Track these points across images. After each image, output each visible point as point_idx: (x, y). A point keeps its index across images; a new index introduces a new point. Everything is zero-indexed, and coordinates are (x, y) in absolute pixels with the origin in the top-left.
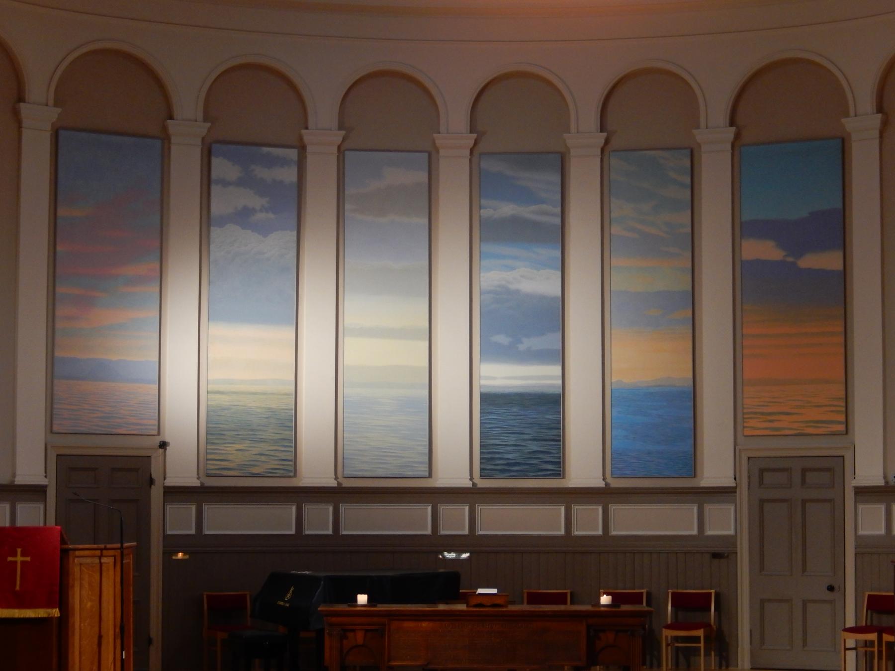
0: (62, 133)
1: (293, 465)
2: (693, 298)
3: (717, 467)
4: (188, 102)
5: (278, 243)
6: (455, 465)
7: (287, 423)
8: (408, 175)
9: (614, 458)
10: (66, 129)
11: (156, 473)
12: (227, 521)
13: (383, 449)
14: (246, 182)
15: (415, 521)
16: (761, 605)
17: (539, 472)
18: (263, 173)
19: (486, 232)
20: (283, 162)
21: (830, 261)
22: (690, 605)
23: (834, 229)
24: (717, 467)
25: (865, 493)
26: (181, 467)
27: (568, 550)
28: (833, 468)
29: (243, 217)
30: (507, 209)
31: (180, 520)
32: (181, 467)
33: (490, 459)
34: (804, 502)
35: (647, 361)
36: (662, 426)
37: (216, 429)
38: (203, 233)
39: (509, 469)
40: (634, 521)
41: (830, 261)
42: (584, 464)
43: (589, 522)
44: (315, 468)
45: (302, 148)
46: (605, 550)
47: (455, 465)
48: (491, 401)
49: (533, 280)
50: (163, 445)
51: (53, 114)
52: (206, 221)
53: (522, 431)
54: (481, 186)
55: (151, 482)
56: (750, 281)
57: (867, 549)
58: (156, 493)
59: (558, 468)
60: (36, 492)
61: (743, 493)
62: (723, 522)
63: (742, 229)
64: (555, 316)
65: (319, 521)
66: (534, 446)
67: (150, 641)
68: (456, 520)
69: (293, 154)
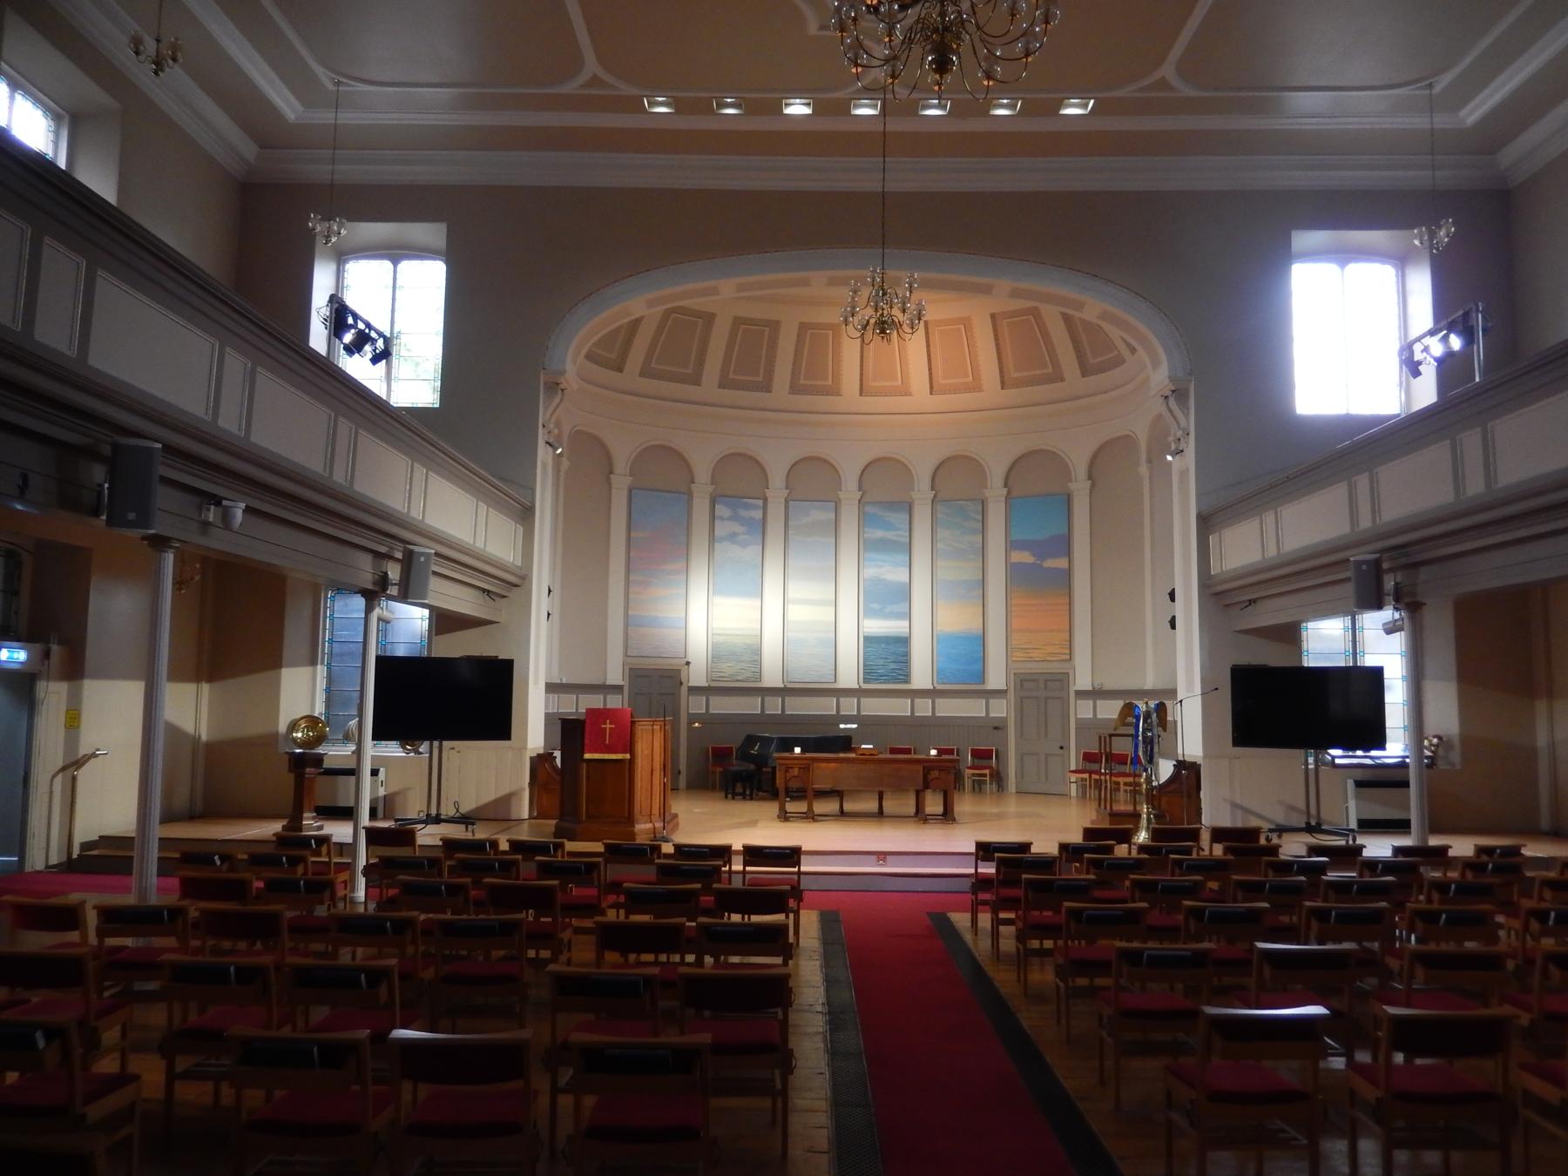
3: (996, 679)
4: (703, 473)
5: (751, 552)
6: (849, 676)
7: (756, 652)
8: (823, 514)
9: (938, 673)
13: (809, 669)
14: (734, 518)
17: (896, 680)
18: (743, 513)
19: (867, 547)
20: (755, 507)
21: (1061, 563)
22: (981, 755)
23: (1064, 545)
24: (996, 679)
25: (1081, 694)
26: (697, 676)
28: (1063, 680)
29: (732, 537)
30: (879, 534)
31: (697, 705)
33: (869, 673)
35: (957, 619)
37: (717, 655)
40: (949, 708)
41: (1061, 563)
42: (921, 676)
43: (924, 708)
44: (771, 679)
45: (765, 500)
47: (849, 676)
48: (870, 640)
49: (890, 571)
50: (688, 663)
51: (629, 480)
52: (712, 539)
53: (887, 658)
54: (864, 520)
57: (1082, 726)
58: (684, 690)
59: (907, 678)
60: (617, 689)
61: (1011, 694)
62: (1000, 709)
63: (1011, 545)
64: (905, 593)
65: (774, 706)
66: (893, 666)
69: (760, 502)
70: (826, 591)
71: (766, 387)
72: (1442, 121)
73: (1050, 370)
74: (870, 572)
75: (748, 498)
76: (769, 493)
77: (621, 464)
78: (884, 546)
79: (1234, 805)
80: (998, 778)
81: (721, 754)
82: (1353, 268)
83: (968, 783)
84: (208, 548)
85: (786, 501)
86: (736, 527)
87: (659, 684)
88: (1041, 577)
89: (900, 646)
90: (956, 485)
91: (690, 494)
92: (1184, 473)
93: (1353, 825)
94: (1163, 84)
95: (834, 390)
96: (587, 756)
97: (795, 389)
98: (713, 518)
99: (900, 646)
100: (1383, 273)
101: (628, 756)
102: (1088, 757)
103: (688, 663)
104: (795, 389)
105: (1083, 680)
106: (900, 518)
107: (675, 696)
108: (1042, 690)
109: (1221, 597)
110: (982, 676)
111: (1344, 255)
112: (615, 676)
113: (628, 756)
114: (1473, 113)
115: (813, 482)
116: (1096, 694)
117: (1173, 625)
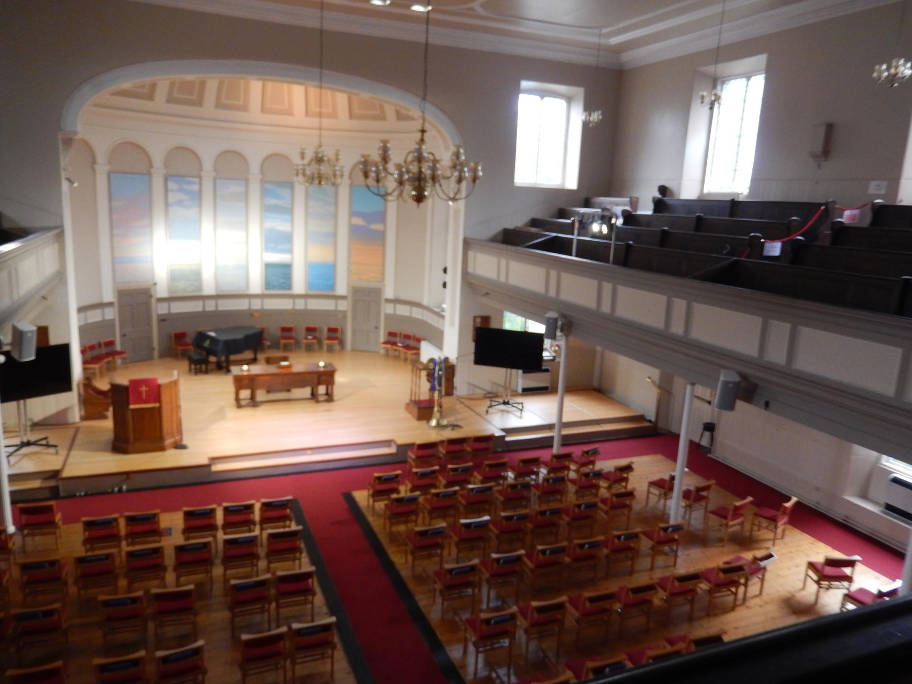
0: (112, 175)
1: (200, 288)
2: (335, 235)
3: (342, 289)
4: (158, 160)
5: (192, 212)
6: (256, 285)
7: (198, 274)
8: (236, 188)
9: (309, 285)
10: (113, 172)
11: (153, 292)
12: (179, 308)
13: (231, 284)
14: (181, 190)
15: (241, 305)
16: (354, 332)
17: (284, 288)
18: (186, 187)
19: (267, 209)
20: (194, 183)
21: (379, 227)
22: (332, 330)
23: (381, 217)
24: (342, 289)
25: (388, 301)
26: (162, 291)
27: (294, 313)
28: (377, 293)
29: (180, 203)
30: (273, 201)
31: (162, 309)
32: (162, 291)
33: (268, 285)
34: (263, 110)
35: (320, 254)
36: (323, 277)
37: (173, 277)
38: (348, 471)
39: (274, 288)
40: (315, 305)
41: (379, 227)
42: (299, 285)
43: (300, 305)
44: (209, 289)
45: (200, 177)
46: (305, 313)
47: (256, 285)
48: (268, 266)
49: (280, 225)
50: (155, 284)
51: (107, 168)
52: (167, 204)
53: (278, 276)
54: (264, 193)
55: (151, 296)
56: (356, 232)
57: (388, 317)
58: (153, 301)
59: (289, 286)
60: (110, 304)
61: (350, 298)
62: (343, 306)
63: (353, 214)
64: (288, 238)
65: (210, 306)
66: (282, 281)
67: (153, 349)
68: (256, 305)
69: (197, 180)
70: (241, 235)
71: (199, 102)
72: (603, 41)
73: (379, 112)
74: (269, 224)
75: (187, 177)
76: (203, 174)
77: (101, 158)
78: (276, 209)
79: (470, 384)
80: (342, 343)
81: (180, 337)
82: (546, 99)
83: (325, 347)
84: (43, 534)
85: (215, 180)
86: (181, 196)
87: (136, 300)
88: (367, 235)
89: (285, 270)
90: (318, 173)
91: (149, 174)
92: (457, 212)
93: (520, 391)
94: (472, 9)
95: (244, 108)
96: (132, 407)
97: (219, 105)
98: (166, 190)
99: (285, 270)
100: (561, 104)
101: (157, 405)
102: (391, 334)
103: (155, 284)
104: (219, 105)
105: (389, 292)
106: (286, 192)
107: (147, 306)
108: (366, 297)
109: (471, 285)
110: (333, 287)
111: (543, 94)
112: (109, 296)
113: (157, 405)
114: (614, 41)
115: (231, 165)
116: (396, 301)
117: (444, 285)
